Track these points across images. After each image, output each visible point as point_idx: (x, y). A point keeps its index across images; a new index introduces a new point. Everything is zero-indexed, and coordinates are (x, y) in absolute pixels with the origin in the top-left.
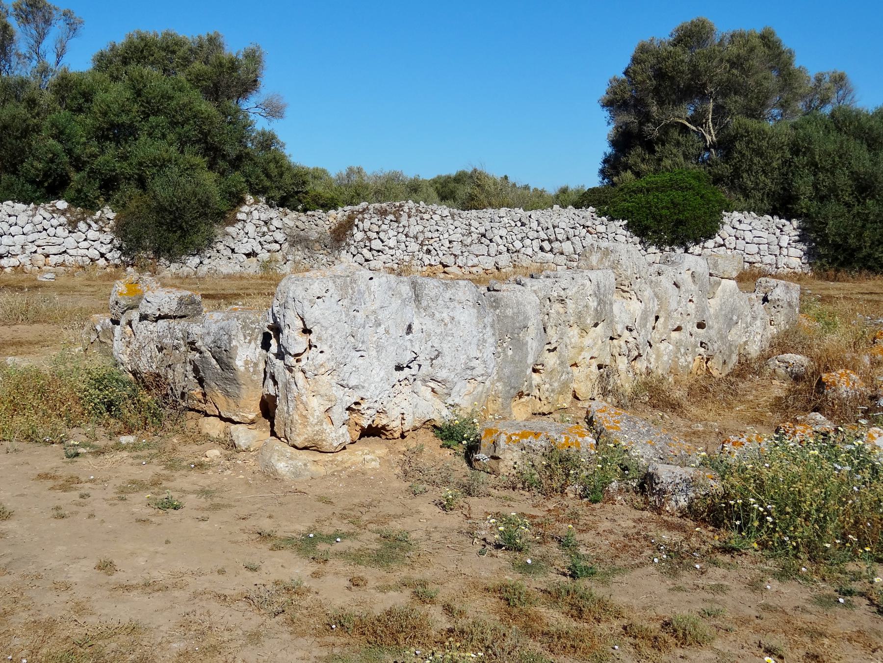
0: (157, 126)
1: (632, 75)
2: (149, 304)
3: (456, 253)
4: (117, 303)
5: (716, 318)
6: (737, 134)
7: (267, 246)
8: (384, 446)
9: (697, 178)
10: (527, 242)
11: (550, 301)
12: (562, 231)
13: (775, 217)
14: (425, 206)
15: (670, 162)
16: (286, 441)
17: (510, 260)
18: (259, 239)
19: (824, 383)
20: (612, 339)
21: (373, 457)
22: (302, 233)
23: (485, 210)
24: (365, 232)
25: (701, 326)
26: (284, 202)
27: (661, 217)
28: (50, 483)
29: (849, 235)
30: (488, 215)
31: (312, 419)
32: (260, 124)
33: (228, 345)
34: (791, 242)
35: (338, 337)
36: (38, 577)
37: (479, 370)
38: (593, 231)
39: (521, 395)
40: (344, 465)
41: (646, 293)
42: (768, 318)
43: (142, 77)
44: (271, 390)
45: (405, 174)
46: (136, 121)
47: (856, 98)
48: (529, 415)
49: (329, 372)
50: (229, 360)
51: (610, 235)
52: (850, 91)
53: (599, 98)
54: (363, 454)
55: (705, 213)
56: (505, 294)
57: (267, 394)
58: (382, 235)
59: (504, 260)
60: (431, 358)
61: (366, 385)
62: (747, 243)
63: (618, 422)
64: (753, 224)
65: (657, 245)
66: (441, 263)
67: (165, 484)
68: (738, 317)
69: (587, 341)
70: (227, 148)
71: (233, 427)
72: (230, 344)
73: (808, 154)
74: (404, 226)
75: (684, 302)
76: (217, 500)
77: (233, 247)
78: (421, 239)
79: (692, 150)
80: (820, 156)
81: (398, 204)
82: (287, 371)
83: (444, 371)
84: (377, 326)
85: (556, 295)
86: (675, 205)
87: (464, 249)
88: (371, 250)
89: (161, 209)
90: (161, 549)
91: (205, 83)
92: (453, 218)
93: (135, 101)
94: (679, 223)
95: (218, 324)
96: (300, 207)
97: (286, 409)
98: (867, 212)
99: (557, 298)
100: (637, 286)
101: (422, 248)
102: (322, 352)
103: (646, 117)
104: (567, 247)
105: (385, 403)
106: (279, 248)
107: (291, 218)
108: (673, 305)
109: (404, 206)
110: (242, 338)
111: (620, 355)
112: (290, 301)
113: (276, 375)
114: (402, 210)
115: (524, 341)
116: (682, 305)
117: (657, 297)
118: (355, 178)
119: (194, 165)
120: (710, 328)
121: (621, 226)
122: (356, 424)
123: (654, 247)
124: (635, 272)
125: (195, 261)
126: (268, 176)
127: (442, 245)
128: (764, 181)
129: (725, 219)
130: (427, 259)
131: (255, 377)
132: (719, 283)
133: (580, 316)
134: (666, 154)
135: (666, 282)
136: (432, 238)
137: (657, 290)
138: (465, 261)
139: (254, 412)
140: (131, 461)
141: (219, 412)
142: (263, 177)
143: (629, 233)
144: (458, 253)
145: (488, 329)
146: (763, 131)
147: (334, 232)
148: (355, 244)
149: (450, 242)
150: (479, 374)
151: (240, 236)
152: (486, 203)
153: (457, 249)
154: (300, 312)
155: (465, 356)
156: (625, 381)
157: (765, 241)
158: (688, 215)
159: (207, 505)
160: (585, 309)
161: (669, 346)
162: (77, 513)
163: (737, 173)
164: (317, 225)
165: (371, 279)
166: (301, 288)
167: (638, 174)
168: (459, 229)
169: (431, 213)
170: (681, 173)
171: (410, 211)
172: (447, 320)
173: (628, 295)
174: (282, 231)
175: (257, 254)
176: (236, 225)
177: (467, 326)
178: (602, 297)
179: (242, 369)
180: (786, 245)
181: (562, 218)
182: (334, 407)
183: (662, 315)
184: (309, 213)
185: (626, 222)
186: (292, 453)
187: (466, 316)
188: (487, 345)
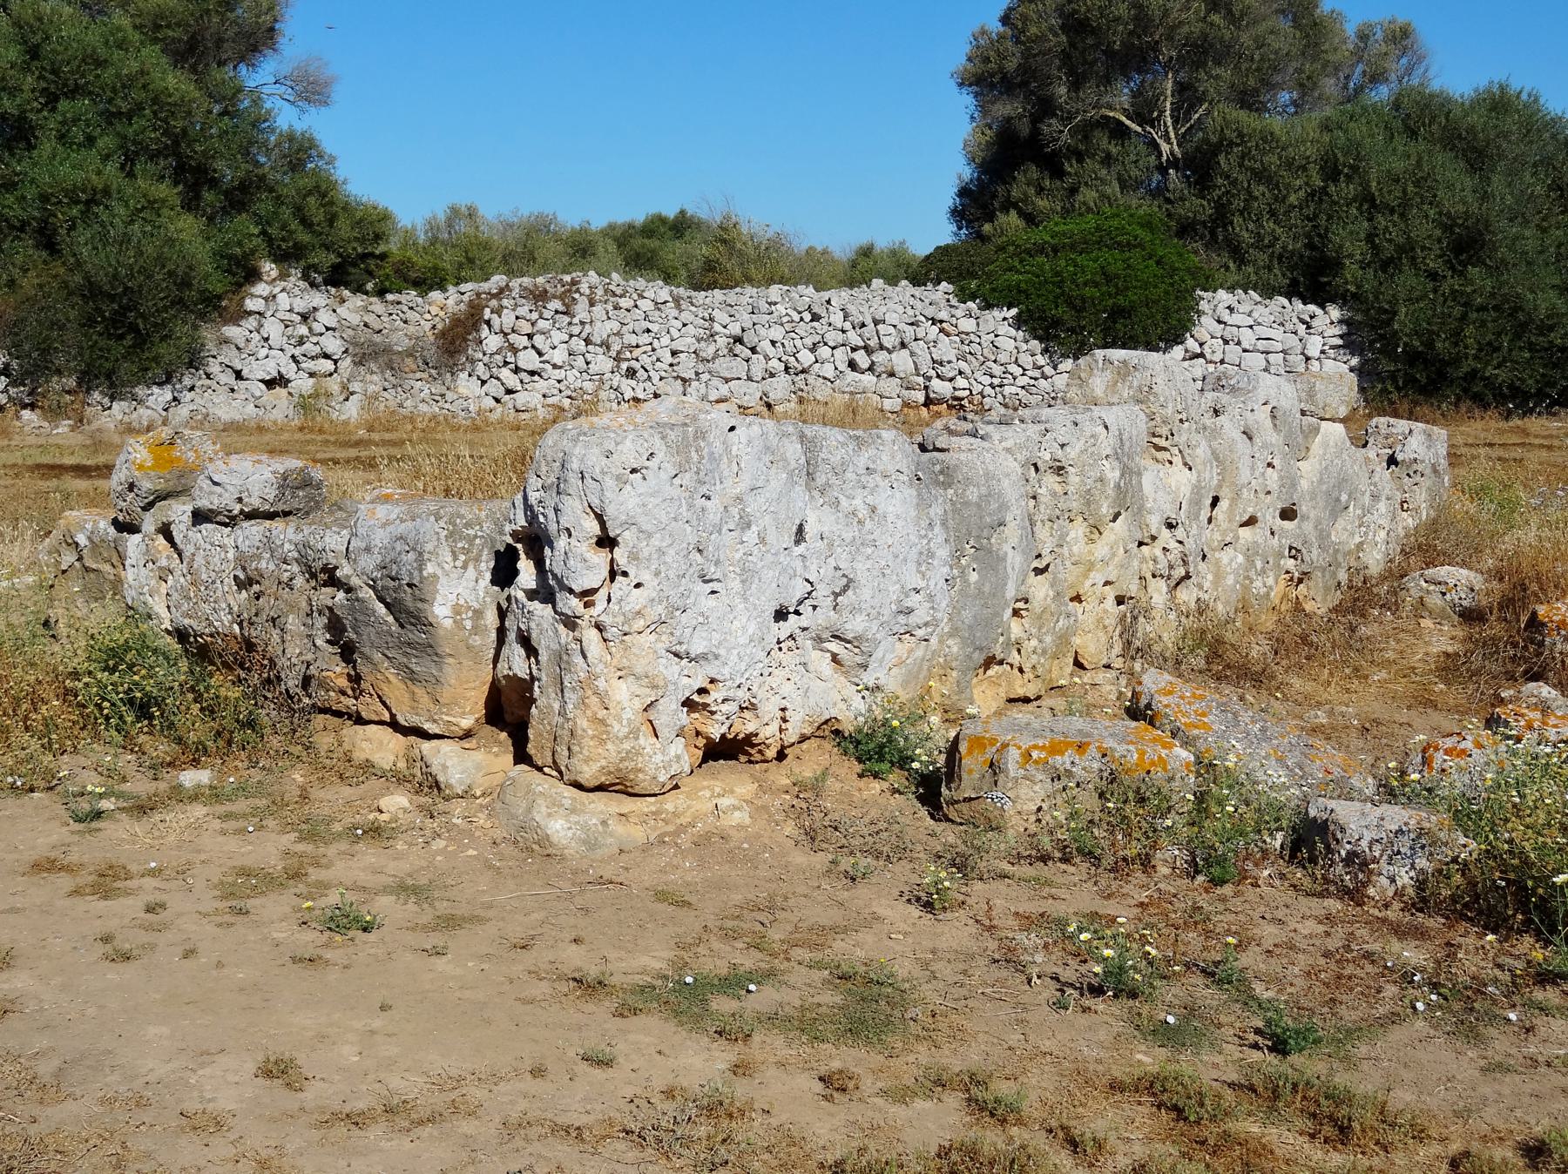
0: (75, 121)
2: (218, 489)
4: (131, 487)
5: (1311, 499)
6: (1221, 142)
7: (309, 365)
8: (745, 776)
9: (1147, 225)
10: (824, 352)
11: (1037, 470)
12: (892, 330)
14: (623, 283)
15: (1094, 194)
16: (554, 773)
18: (291, 350)
19: (1543, 624)
20: (1141, 544)
21: (736, 802)
22: (377, 338)
23: (738, 290)
24: (506, 335)
25: (1288, 514)
26: (339, 277)
28: (65, 882)
30: (745, 300)
31: (617, 727)
32: (287, 118)
33: (416, 573)
34: (1326, 348)
35: (672, 552)
36: (141, 1103)
37: (922, 615)
39: (989, 662)
40: (678, 822)
41: (1199, 451)
42: (1399, 496)
43: (40, 19)
44: (516, 662)
45: (561, 218)
46: (32, 109)
47: (1431, 74)
48: (1001, 702)
49: (653, 627)
50: (420, 605)
51: (984, 337)
52: (1421, 59)
53: (953, 69)
54: (712, 796)
55: (1167, 293)
56: (963, 456)
57: (506, 677)
58: (539, 340)
60: (833, 593)
61: (722, 652)
62: (1245, 351)
63: (1204, 715)
64: (1256, 315)
67: (314, 874)
68: (1350, 496)
69: (1101, 549)
70: (220, 165)
71: (426, 746)
72: (421, 571)
73: (1357, 180)
74: (582, 323)
75: (1261, 466)
76: (443, 907)
78: (616, 347)
79: (1135, 172)
80: (1379, 183)
81: (567, 278)
82: (561, 627)
83: (860, 618)
84: (743, 529)
85: (1047, 457)
86: (1109, 278)
87: (701, 368)
88: (517, 370)
89: (92, 291)
90: (377, 1024)
91: (171, 33)
92: (678, 306)
93: (26, 68)
95: (389, 529)
96: (369, 286)
97: (556, 706)
99: (1051, 464)
100: (1184, 438)
101: (618, 367)
102: (638, 586)
103: (1046, 107)
104: (902, 361)
105: (754, 689)
107: (354, 308)
108: (1245, 475)
109: (578, 282)
110: (449, 559)
111: (1154, 576)
112: (573, 479)
113: (534, 635)
114: (578, 291)
115: (1001, 553)
116: (1257, 473)
117: (1217, 459)
118: (462, 227)
119: (155, 201)
120: (1305, 518)
121: (1005, 319)
122: (698, 733)
124: (1180, 408)
125: (161, 395)
126: (306, 223)
128: (1274, 230)
129: (1203, 305)
131: (476, 641)
132: (1317, 430)
133: (1088, 499)
134: (1087, 178)
135: (1229, 426)
136: (637, 346)
137: (1215, 444)
139: (471, 713)
140: (217, 824)
141: (393, 716)
142: (294, 225)
144: (689, 374)
145: (937, 529)
146: (1272, 134)
148: (486, 359)
149: (674, 353)
150: (920, 622)
151: (252, 346)
152: (738, 274)
153: (687, 366)
154: (595, 502)
155: (898, 586)
156: (1163, 629)
157: (1279, 347)
159: (426, 918)
160: (1099, 484)
161: (1236, 557)
162: (153, 947)
163: (1222, 215)
164: (405, 322)
165: (732, 429)
166: (596, 450)
167: (1030, 219)
168: (690, 329)
169: (635, 296)
170: (1118, 216)
171: (592, 293)
172: (863, 512)
173: (1166, 455)
174: (337, 334)
175: (288, 381)
176: (243, 323)
177: (900, 524)
178: (1125, 459)
179: (448, 623)
180: (1316, 354)
181: (891, 304)
182: (661, 701)
184: (390, 297)
185: (1014, 311)
186: (574, 799)
187: (897, 503)
188: (935, 563)
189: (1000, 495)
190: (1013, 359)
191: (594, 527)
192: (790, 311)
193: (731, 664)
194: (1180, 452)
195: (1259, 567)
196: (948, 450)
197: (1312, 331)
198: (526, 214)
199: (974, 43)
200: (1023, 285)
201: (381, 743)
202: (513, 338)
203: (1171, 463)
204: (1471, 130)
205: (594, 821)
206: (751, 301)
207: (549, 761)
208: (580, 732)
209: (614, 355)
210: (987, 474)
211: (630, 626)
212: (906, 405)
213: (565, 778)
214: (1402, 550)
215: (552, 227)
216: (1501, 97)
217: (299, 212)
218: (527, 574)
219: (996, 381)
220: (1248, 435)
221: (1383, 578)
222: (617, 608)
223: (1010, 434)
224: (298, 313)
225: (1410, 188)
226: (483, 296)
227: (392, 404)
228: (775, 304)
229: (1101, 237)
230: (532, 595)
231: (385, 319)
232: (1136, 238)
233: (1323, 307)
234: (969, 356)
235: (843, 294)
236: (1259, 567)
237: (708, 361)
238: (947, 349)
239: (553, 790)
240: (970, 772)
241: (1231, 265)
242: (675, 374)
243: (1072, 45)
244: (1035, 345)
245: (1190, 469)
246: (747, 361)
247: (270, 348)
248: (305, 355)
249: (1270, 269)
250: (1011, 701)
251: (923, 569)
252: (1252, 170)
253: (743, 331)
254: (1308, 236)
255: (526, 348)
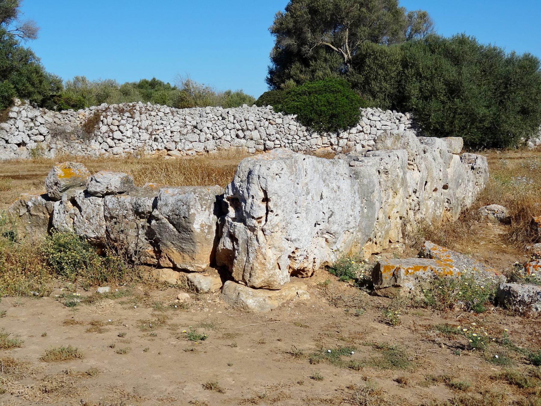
1: (293, 10)
2: (98, 184)
3: (176, 140)
6: (366, 53)
10: (227, 131)
12: (252, 123)
13: (394, 111)
14: (152, 106)
15: (321, 73)
16: (243, 283)
17: (215, 144)
18: (27, 132)
22: (59, 127)
24: (109, 126)
25: (445, 187)
27: (321, 112)
29: (445, 123)
30: (197, 112)
31: (269, 265)
32: (25, 44)
33: (187, 213)
34: (406, 128)
37: (352, 224)
38: (273, 123)
44: (226, 243)
50: (188, 224)
51: (285, 125)
53: (269, 27)
55: (350, 109)
59: (211, 145)
61: (301, 238)
62: (378, 130)
64: (381, 116)
65: (318, 132)
66: (166, 148)
69: (396, 201)
71: (190, 276)
72: (189, 212)
74: (138, 121)
75: (438, 170)
77: (7, 139)
78: (150, 130)
79: (336, 65)
80: (422, 69)
81: (131, 104)
82: (248, 231)
83: (336, 225)
84: (307, 195)
85: (383, 168)
86: (330, 103)
87: (182, 137)
88: (113, 139)
92: (173, 115)
94: (333, 116)
95: (174, 197)
96: (55, 107)
97: (245, 259)
98: (455, 107)
101: (151, 137)
103: (303, 41)
104: (255, 134)
106: (43, 139)
107: (50, 116)
110: (200, 207)
113: (237, 234)
115: (374, 202)
118: (80, 85)
120: (450, 188)
121: (292, 119)
122: (290, 267)
123: (316, 133)
126: (33, 85)
127: (166, 135)
129: (363, 113)
130: (155, 145)
131: (209, 237)
136: (158, 130)
138: (183, 146)
139: (206, 263)
143: (298, 124)
144: (177, 140)
145: (357, 194)
146: (385, 51)
147: (85, 125)
149: (172, 132)
150: (352, 227)
152: (193, 103)
153: (177, 137)
154: (264, 186)
155: (347, 214)
158: (339, 111)
163: (367, 82)
164: (70, 121)
165: (304, 159)
167: (298, 82)
169: (157, 111)
172: (336, 188)
173: (412, 167)
176: (8, 122)
177: (346, 192)
179: (198, 231)
181: (250, 113)
183: (429, 180)
184: (63, 112)
185: (296, 116)
186: (253, 292)
187: (346, 184)
188: (356, 206)
189: (373, 181)
190: (296, 133)
191: (262, 195)
192: (214, 116)
193: (303, 242)
194: (417, 165)
195: (438, 206)
196: (354, 166)
197: (401, 122)
198: (104, 80)
199: (276, 17)
200: (299, 106)
201: (170, 275)
202: (111, 127)
203: (414, 169)
204: (453, 50)
205: (261, 299)
206: (199, 112)
207: (241, 279)
208: (255, 268)
209: (150, 133)
210: (369, 174)
211: (274, 229)
212: (257, 150)
213: (248, 285)
214: (477, 199)
215: (114, 84)
216: (463, 39)
217: (29, 79)
218: (232, 212)
219: (290, 141)
220: (434, 159)
221: (471, 209)
222: (269, 223)
223: (371, 160)
224: (30, 118)
225: (434, 71)
226: (100, 111)
227: (67, 152)
228: (209, 113)
229: (326, 88)
230: (234, 219)
231: (62, 120)
232: (338, 89)
233: (403, 113)
234: (280, 133)
235: (233, 110)
236: (438, 206)
237: (184, 135)
238: (272, 130)
239: (245, 289)
240: (386, 278)
241: (371, 99)
242: (172, 140)
243: (312, 18)
244: (304, 128)
245: (420, 172)
246: (199, 135)
247: (19, 131)
248: (33, 134)
249: (384, 100)
250: (373, 254)
251: (353, 208)
252: (378, 65)
253: (197, 123)
254: (398, 88)
255: (116, 131)
